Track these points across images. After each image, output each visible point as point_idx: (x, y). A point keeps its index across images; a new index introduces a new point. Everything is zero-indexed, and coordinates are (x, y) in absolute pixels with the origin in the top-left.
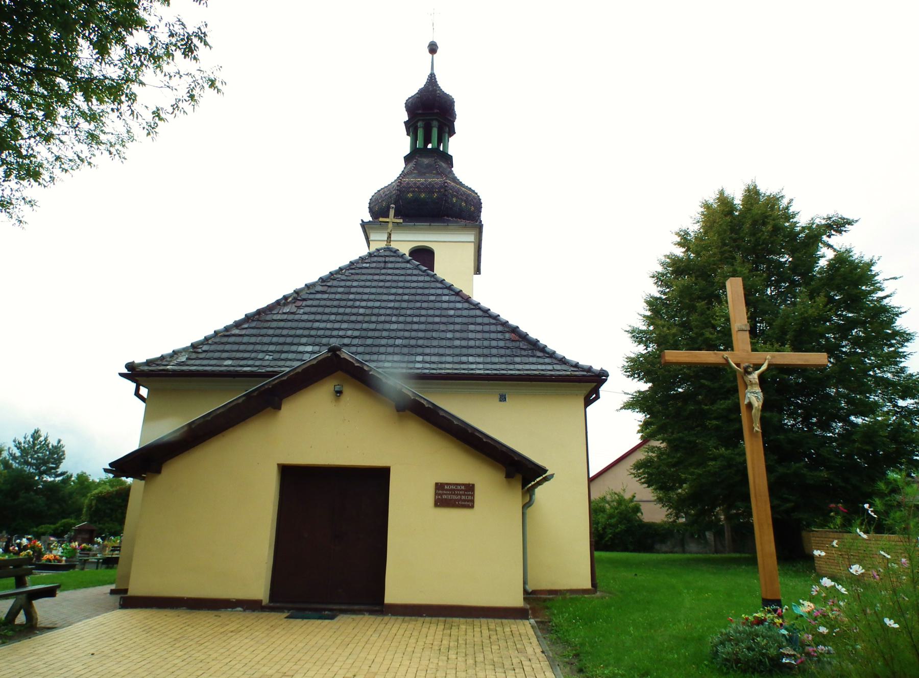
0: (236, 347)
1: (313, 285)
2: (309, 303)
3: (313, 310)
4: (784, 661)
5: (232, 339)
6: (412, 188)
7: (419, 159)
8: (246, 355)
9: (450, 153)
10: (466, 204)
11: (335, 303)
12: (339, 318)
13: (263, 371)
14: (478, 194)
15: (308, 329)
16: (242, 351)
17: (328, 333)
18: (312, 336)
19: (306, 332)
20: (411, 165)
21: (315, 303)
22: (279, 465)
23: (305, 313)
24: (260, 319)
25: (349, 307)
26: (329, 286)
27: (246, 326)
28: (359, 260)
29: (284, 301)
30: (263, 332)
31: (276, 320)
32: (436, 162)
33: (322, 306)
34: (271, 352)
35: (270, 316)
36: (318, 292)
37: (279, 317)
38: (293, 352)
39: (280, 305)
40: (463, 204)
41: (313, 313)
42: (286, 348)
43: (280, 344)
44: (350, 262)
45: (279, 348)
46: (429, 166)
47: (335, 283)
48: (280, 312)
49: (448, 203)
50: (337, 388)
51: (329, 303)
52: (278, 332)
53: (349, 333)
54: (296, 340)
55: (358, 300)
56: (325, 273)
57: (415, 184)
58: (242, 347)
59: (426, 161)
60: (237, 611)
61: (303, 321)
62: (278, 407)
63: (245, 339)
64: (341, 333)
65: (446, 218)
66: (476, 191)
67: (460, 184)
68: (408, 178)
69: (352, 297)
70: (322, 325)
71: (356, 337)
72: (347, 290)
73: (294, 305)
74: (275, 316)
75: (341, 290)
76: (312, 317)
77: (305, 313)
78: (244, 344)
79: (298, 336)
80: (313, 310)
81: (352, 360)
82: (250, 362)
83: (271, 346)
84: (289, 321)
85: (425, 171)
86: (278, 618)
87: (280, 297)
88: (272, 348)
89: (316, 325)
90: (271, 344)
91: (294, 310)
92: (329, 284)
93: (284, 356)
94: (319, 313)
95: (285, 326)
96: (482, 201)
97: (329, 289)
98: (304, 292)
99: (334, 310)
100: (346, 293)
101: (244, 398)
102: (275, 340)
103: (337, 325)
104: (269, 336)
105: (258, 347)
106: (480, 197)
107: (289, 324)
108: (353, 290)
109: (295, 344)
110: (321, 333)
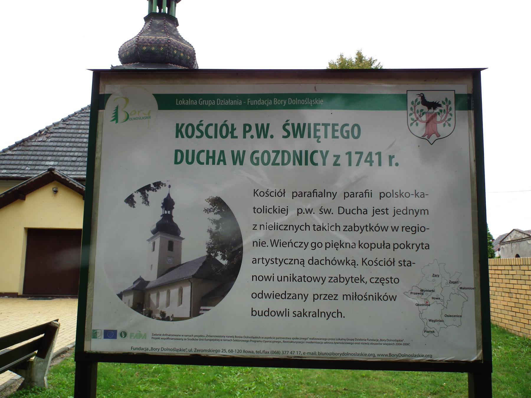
0: (9, 162)
1: (58, 123)
2: (54, 135)
3: (57, 139)
4: (482, 363)
5: (7, 157)
6: (146, 43)
7: (153, 20)
8: (15, 167)
9: (176, 17)
10: (184, 55)
11: (70, 135)
12: (71, 144)
13: (24, 176)
14: (194, 47)
15: (52, 151)
16: (12, 165)
17: (64, 154)
18: (54, 156)
19: (51, 153)
20: (148, 24)
21: (58, 135)
22: (25, 228)
23: (51, 141)
24: (24, 145)
25: (78, 138)
26: (67, 124)
27: (15, 149)
28: (87, 107)
29: (39, 134)
30: (26, 153)
31: (33, 146)
32: (164, 23)
33: (62, 137)
34: (30, 165)
35: (31, 143)
36: (60, 128)
37: (36, 144)
38: (42, 165)
39: (36, 136)
40: (182, 55)
41: (56, 142)
42: (38, 163)
43: (35, 160)
44: (69, 116)
45: (34, 163)
46: (160, 26)
47: (71, 122)
48: (37, 140)
49: (171, 54)
50: (54, 190)
51: (66, 135)
52: (35, 153)
53: (76, 154)
54: (45, 158)
55: (84, 133)
56: (65, 116)
57: (148, 40)
58: (13, 162)
59: (158, 22)
60: (5, 298)
61: (50, 146)
62: (24, 199)
63: (15, 157)
64: (72, 154)
65: (170, 64)
66: (192, 45)
67: (182, 39)
68: (144, 36)
69: (80, 131)
70: (61, 149)
71: (79, 157)
72: (78, 127)
73: (45, 136)
74: (33, 143)
75: (74, 127)
76: (55, 144)
77: (51, 141)
78: (14, 160)
79: (46, 156)
80: (57, 139)
81: (60, 175)
82: (17, 171)
83: (30, 161)
84: (42, 146)
85: (157, 30)
86: (25, 300)
87: (37, 131)
88: (30, 163)
89: (57, 149)
90: (30, 160)
91: (45, 139)
92: (67, 123)
93: (37, 167)
94: (60, 142)
95: (39, 149)
96: (196, 52)
97: (68, 126)
98: (52, 128)
99: (69, 140)
100: (77, 129)
101: (4, 195)
102: (32, 158)
103: (69, 149)
104: (29, 155)
105: (22, 162)
106: (195, 49)
107: (41, 148)
108: (82, 127)
109: (44, 161)
110: (60, 153)
